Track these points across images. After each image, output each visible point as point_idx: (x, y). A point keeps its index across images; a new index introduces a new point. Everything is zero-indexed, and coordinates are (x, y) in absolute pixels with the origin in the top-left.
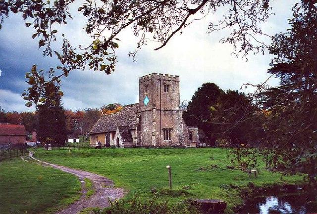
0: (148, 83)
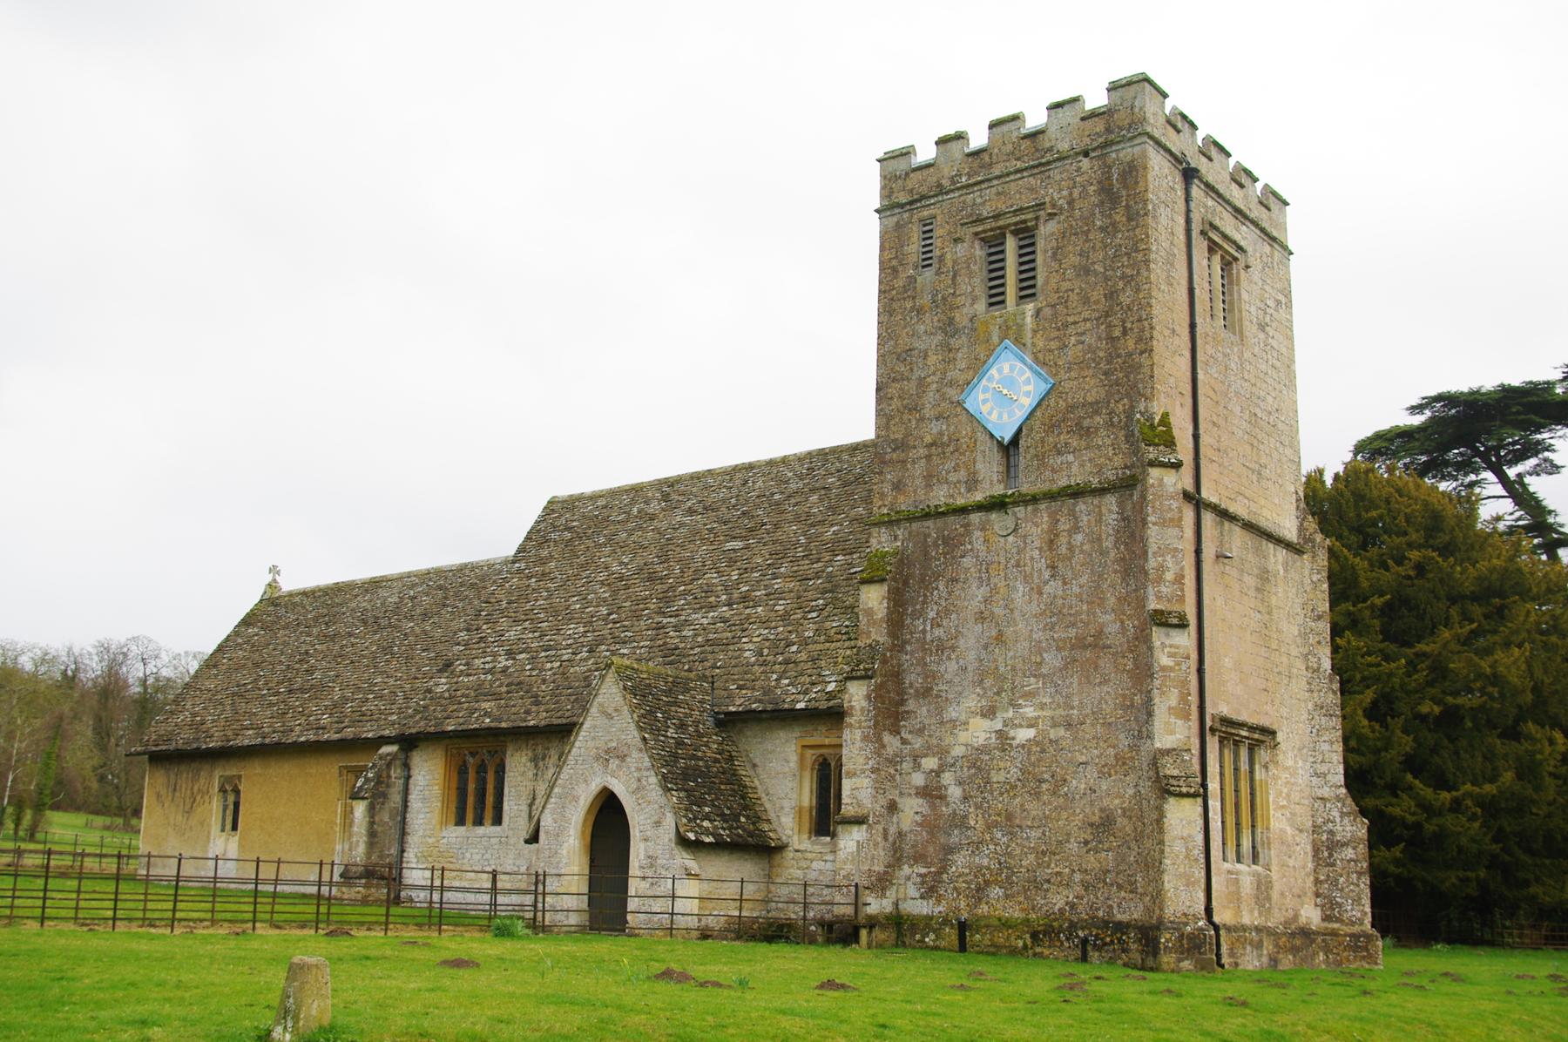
0: (1020, 194)
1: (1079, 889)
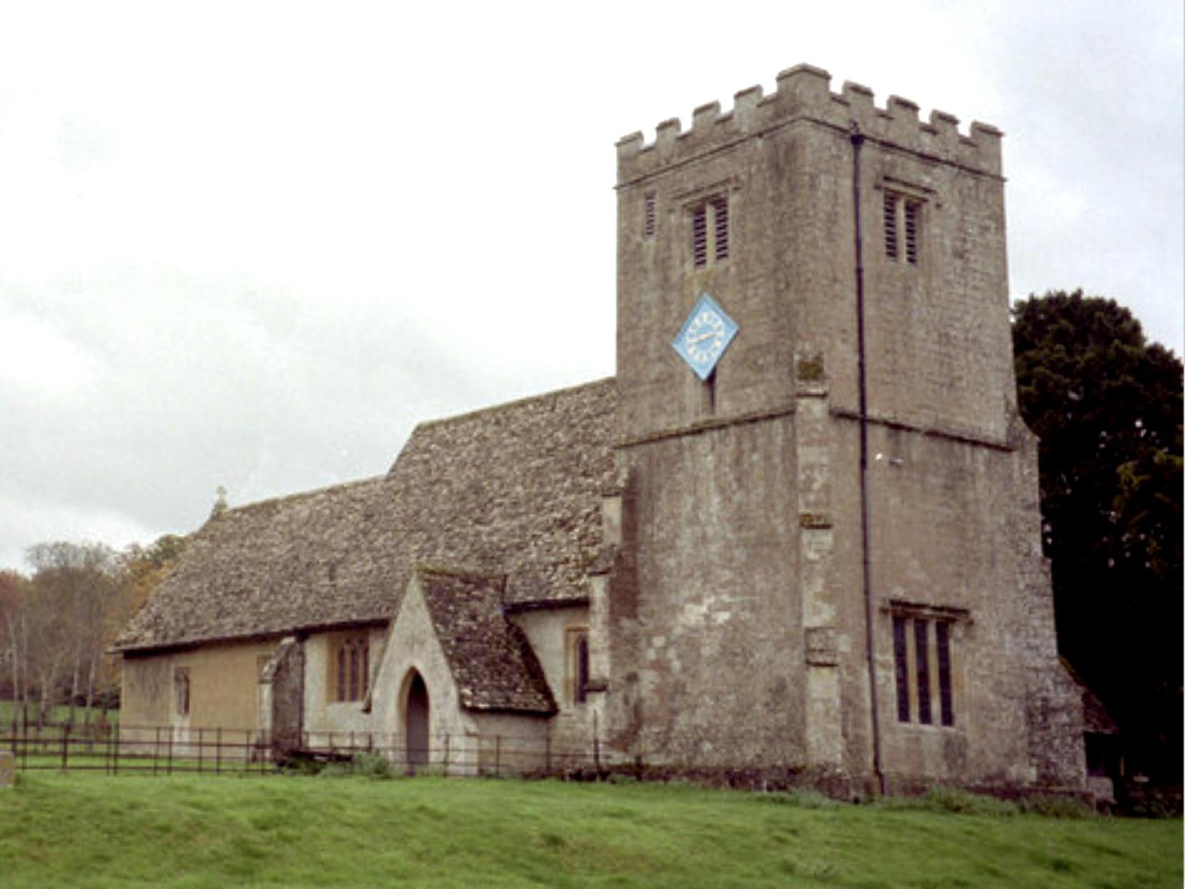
0: (721, 168)
1: (763, 744)
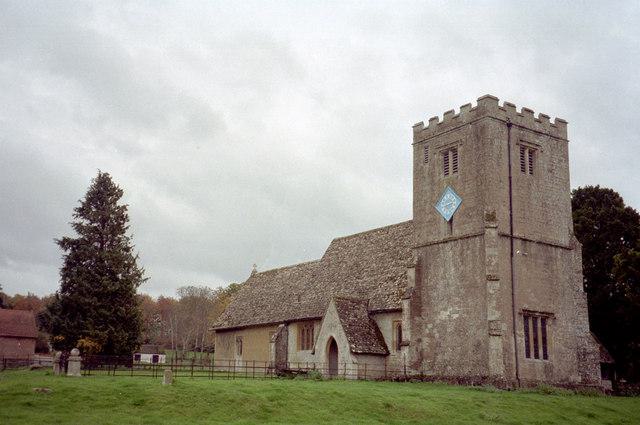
0: (455, 137)
